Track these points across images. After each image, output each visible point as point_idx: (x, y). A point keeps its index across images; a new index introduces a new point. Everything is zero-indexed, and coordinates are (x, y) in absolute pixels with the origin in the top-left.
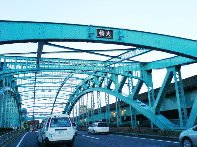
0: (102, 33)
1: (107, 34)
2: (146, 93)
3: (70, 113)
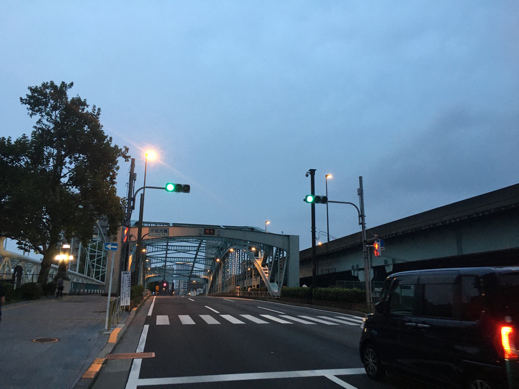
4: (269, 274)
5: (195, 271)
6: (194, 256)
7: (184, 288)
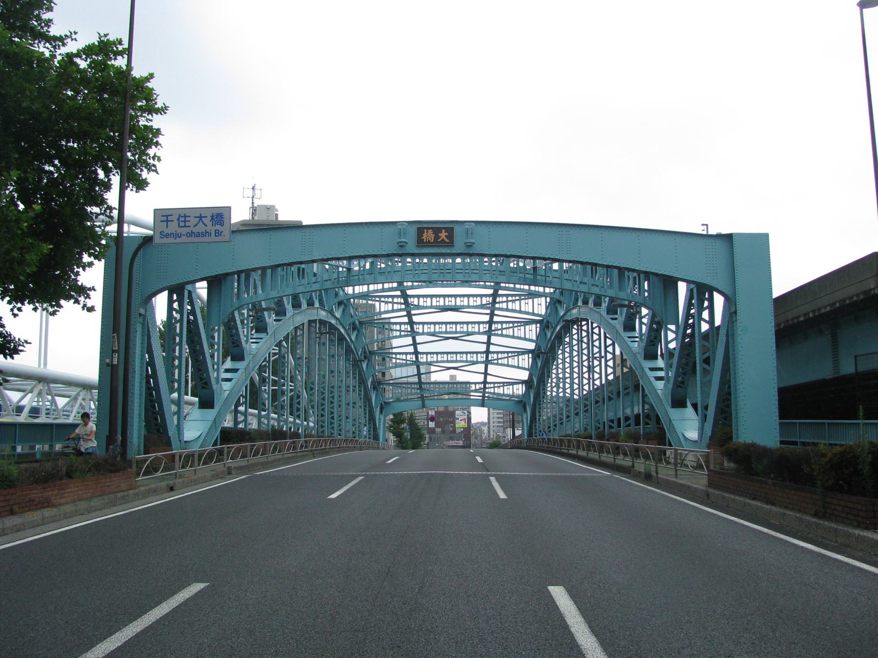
0: (429, 234)
1: (441, 237)
3: (549, 376)
4: (668, 381)
5: (491, 383)
6: (483, 348)
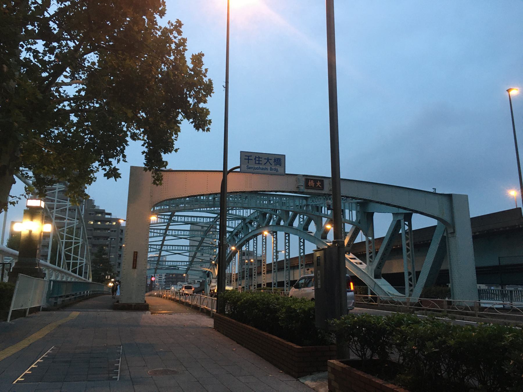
2: (363, 243)
7: (159, 282)
